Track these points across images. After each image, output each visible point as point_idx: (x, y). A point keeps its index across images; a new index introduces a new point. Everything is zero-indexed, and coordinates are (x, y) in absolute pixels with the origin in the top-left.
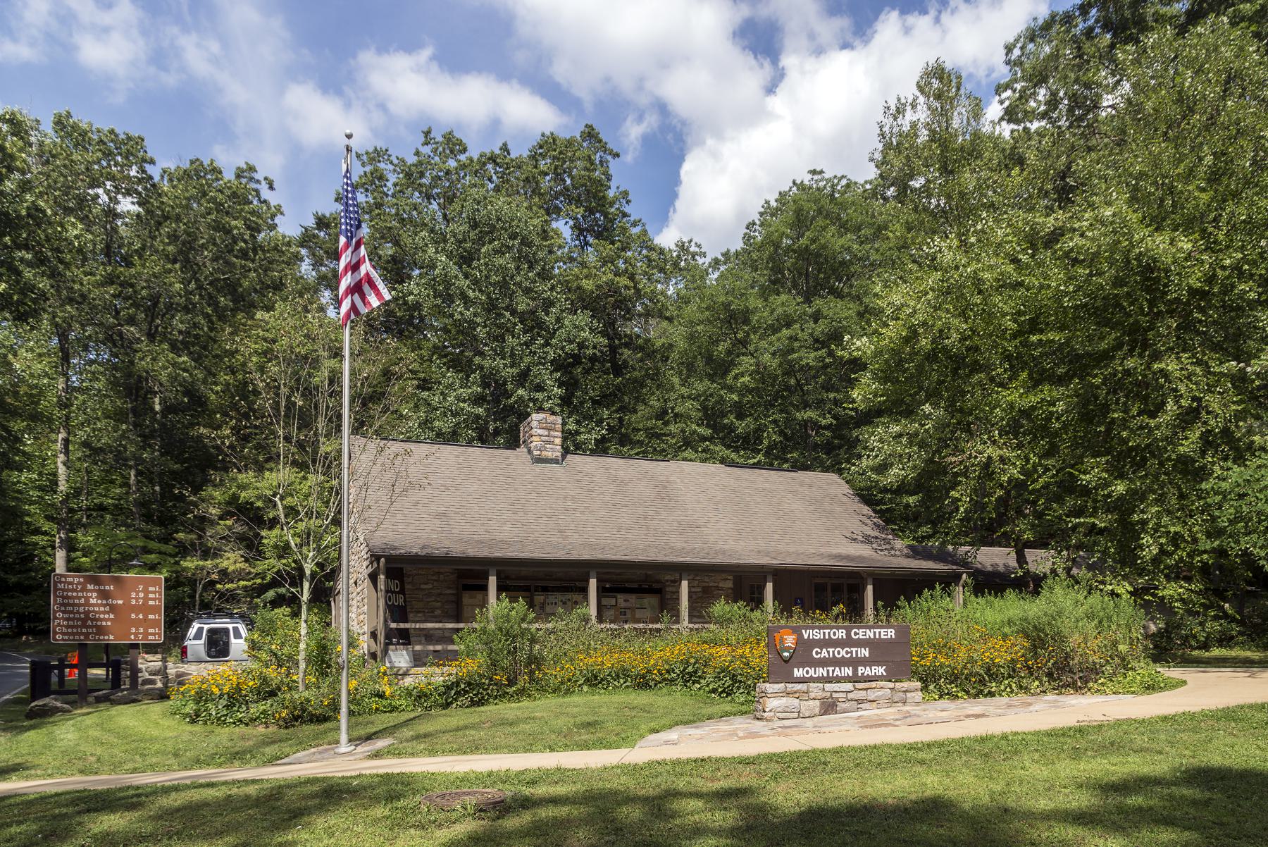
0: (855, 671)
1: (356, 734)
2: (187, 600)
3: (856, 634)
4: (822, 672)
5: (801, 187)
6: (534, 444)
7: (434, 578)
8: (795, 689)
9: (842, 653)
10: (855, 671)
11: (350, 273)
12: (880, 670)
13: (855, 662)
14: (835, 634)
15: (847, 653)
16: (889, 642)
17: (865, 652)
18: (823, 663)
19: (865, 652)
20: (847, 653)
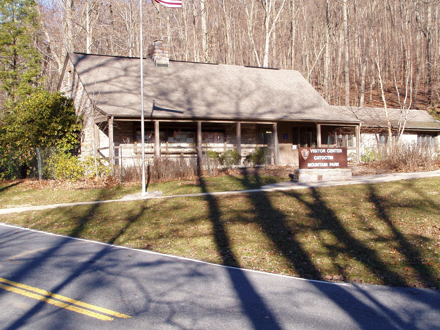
0: (329, 164)
1: (224, 62)
2: (10, 144)
3: (329, 151)
4: (317, 165)
5: (56, 317)
6: (156, 57)
7: (123, 125)
8: (309, 171)
9: (324, 158)
10: (329, 164)
11: (141, 165)
12: (337, 164)
13: (328, 161)
14: (321, 151)
15: (326, 158)
16: (340, 154)
17: (331, 158)
18: (318, 161)
19: (331, 158)
20: (326, 158)
